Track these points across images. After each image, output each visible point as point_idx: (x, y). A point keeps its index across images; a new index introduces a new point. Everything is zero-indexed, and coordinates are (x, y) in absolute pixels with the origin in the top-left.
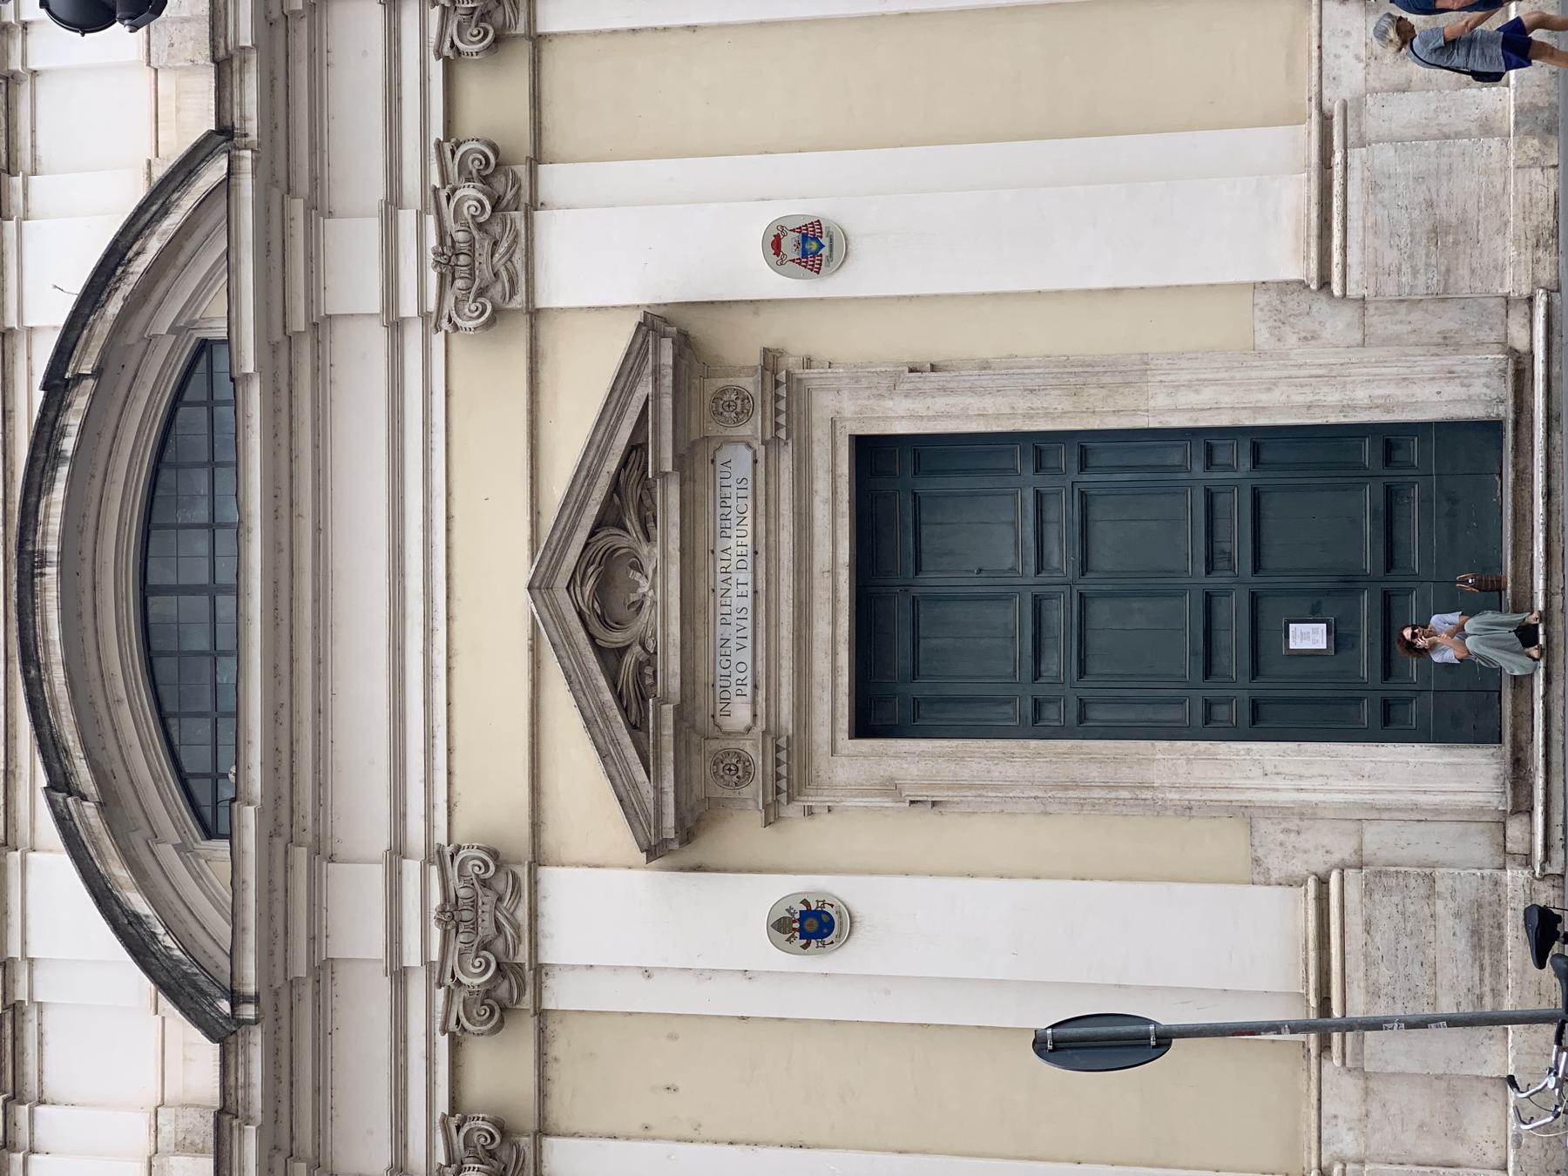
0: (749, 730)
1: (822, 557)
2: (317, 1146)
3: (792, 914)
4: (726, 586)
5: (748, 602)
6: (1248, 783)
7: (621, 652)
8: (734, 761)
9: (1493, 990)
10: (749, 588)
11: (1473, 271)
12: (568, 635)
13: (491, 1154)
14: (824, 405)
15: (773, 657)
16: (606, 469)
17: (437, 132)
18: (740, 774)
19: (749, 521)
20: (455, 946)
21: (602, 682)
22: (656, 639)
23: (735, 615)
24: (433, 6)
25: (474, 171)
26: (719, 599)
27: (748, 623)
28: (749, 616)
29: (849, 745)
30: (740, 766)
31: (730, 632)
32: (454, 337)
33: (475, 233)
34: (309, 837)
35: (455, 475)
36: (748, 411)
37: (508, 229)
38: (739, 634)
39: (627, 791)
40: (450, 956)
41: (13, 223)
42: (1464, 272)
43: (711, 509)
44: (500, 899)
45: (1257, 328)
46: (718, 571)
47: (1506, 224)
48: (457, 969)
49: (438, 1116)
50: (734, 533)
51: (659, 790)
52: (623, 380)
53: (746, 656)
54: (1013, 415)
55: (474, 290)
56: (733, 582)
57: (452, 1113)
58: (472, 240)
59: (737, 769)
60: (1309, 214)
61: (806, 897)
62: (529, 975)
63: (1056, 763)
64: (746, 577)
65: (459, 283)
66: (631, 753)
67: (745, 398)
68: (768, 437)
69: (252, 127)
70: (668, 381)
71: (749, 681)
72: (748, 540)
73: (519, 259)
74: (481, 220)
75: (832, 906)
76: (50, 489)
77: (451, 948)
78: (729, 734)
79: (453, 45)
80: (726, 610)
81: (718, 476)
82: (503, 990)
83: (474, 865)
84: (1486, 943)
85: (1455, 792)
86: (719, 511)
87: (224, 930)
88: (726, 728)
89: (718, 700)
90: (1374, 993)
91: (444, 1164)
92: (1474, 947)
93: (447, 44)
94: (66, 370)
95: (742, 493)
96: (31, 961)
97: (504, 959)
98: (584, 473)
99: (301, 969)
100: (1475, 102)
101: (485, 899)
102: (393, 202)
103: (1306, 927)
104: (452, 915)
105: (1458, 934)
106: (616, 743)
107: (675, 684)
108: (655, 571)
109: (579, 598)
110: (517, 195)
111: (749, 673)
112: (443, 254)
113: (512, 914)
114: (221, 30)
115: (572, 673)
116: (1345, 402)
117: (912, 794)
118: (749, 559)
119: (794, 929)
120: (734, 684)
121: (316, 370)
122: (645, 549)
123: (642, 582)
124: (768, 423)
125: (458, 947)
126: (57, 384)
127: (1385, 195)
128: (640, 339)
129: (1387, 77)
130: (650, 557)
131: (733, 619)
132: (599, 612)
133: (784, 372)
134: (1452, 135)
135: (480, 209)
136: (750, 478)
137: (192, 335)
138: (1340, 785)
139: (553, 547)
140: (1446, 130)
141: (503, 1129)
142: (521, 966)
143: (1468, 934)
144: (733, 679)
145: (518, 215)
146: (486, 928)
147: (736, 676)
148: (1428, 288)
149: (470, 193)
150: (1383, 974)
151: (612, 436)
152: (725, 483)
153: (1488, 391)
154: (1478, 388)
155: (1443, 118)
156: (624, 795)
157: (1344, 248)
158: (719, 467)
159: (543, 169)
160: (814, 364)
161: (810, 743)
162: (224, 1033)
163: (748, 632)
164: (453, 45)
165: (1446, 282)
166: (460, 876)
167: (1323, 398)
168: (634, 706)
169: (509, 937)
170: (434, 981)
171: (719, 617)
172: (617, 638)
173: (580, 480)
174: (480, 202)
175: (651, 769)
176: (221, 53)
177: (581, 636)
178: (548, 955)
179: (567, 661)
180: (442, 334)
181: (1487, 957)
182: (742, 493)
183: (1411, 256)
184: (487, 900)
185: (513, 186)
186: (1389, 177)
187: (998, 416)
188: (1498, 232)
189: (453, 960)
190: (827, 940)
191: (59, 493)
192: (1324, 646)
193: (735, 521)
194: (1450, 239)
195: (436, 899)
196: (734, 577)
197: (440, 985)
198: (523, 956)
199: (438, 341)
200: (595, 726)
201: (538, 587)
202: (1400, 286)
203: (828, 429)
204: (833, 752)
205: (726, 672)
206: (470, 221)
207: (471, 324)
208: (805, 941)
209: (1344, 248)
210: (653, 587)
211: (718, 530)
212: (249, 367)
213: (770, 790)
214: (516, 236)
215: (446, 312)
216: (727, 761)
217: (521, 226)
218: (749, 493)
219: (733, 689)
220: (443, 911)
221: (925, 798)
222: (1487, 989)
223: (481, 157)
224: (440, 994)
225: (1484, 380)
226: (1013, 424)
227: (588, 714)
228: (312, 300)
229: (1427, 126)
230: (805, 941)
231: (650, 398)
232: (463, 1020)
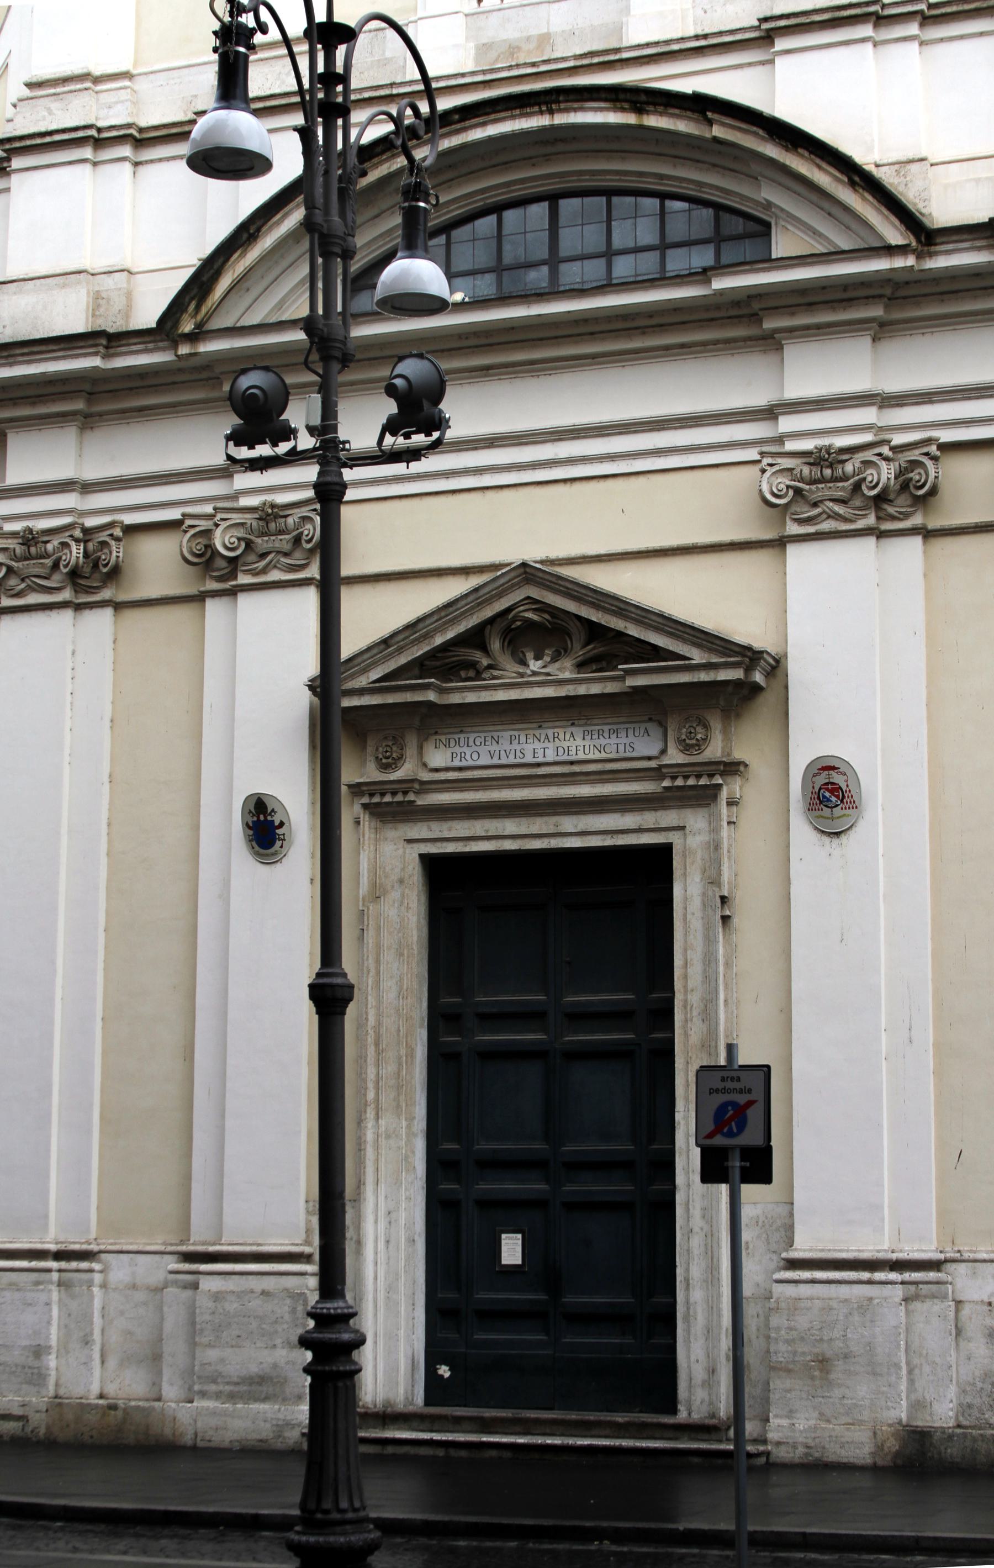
0: (425, 765)
1: (569, 823)
2: (100, 415)
3: (270, 814)
4: (543, 737)
5: (529, 759)
6: (381, 1199)
7: (485, 649)
8: (394, 755)
9: (221, 1392)
10: (540, 759)
11: (789, 1391)
12: (488, 601)
13: (96, 566)
14: (695, 820)
15: (483, 784)
16: (629, 625)
17: (947, 436)
18: (384, 761)
19: (598, 756)
20: (248, 518)
21: (450, 634)
22: (491, 679)
23: (518, 748)
25: (911, 475)
26: (531, 732)
27: (512, 760)
28: (518, 761)
29: (414, 855)
30: (390, 760)
31: (505, 744)
32: (756, 469)
33: (851, 481)
35: (641, 480)
36: (687, 750)
37: (857, 512)
40: (240, 515)
42: (788, 1383)
43: (610, 720)
44: (286, 555)
45: (758, 1206)
46: (556, 730)
47: (828, 1421)
48: (228, 523)
49: (887, 437)
50: (587, 743)
51: (361, 692)
52: (702, 636)
53: (484, 760)
54: (686, 991)
55: (800, 485)
56: (546, 744)
58: (845, 478)
59: (387, 758)
60: (848, 1251)
61: (287, 824)
62: (227, 585)
63: (398, 1035)
65: (806, 470)
66: (392, 665)
67: (698, 746)
68: (664, 770)
70: (704, 676)
71: (464, 763)
72: (581, 756)
73: (827, 526)
74: (864, 487)
75: (281, 847)
76: (615, 109)
77: (10, 541)
78: (422, 748)
80: (523, 739)
81: (636, 725)
84: (254, 1388)
85: (375, 1367)
86: (606, 728)
87: (254, 318)
88: (425, 744)
89: (449, 736)
90: (217, 1297)
91: (893, 443)
92: (251, 1378)
95: (621, 748)
96: (771, 62)
97: (240, 562)
98: (622, 606)
99: (769, 324)
100: (940, 1397)
101: (284, 542)
103: (270, 1245)
105: (261, 1366)
106: (400, 650)
107: (456, 699)
108: (548, 674)
110: (893, 518)
111: (471, 763)
112: (829, 454)
113: (275, 567)
115: (454, 608)
116: (691, 1282)
118: (565, 758)
119: (258, 817)
120: (462, 750)
121: (727, 341)
122: (568, 663)
123: (539, 663)
124: (676, 770)
125: (247, 521)
127: (856, 1318)
128: (737, 649)
129: (973, 1320)
131: (515, 746)
132: (513, 627)
133: (721, 782)
134: (912, 1377)
135: (872, 485)
136: (635, 754)
137: (772, 217)
138: (381, 1274)
139: (560, 582)
140: (917, 1371)
141: (115, 574)
142: (236, 578)
143: (261, 1373)
144: (465, 749)
145: (871, 520)
146: (262, 543)
147: (468, 752)
148: (776, 1353)
149: (886, 473)
150: (232, 1306)
151: (658, 629)
152: (631, 732)
153: (698, 1402)
154: (700, 1395)
155: (927, 1369)
156: (356, 662)
157: (813, 1281)
158: (643, 726)
159: (917, 541)
160: (735, 808)
161: (414, 821)
163: (504, 761)
165: (780, 1369)
167: (695, 1262)
168: (438, 663)
171: (516, 733)
172: (495, 645)
174: (877, 484)
175: (377, 685)
177: (488, 612)
178: (244, 600)
181: (245, 1388)
182: (621, 748)
183: (802, 1339)
184: (283, 542)
185: (900, 513)
186: (872, 1321)
187: (685, 977)
188: (821, 1414)
192: (504, 1262)
193: (597, 742)
194: (817, 1373)
196: (551, 745)
197: (762, 454)
200: (411, 632)
202: (778, 1329)
204: (409, 841)
205: (471, 743)
206: (861, 476)
207: (765, 488)
208: (251, 825)
209: (813, 1281)
210: (534, 674)
211: (589, 728)
213: (372, 788)
214: (851, 521)
215: (779, 460)
216: (395, 748)
217: (860, 524)
218: (622, 755)
219: (457, 750)
220: (273, 506)
221: (366, 923)
222: (221, 1388)
223: (923, 481)
224: (208, 509)
225: (707, 1399)
226: (679, 991)
228: (791, 331)
229: (921, 1355)
230: (251, 825)
232: (192, 532)
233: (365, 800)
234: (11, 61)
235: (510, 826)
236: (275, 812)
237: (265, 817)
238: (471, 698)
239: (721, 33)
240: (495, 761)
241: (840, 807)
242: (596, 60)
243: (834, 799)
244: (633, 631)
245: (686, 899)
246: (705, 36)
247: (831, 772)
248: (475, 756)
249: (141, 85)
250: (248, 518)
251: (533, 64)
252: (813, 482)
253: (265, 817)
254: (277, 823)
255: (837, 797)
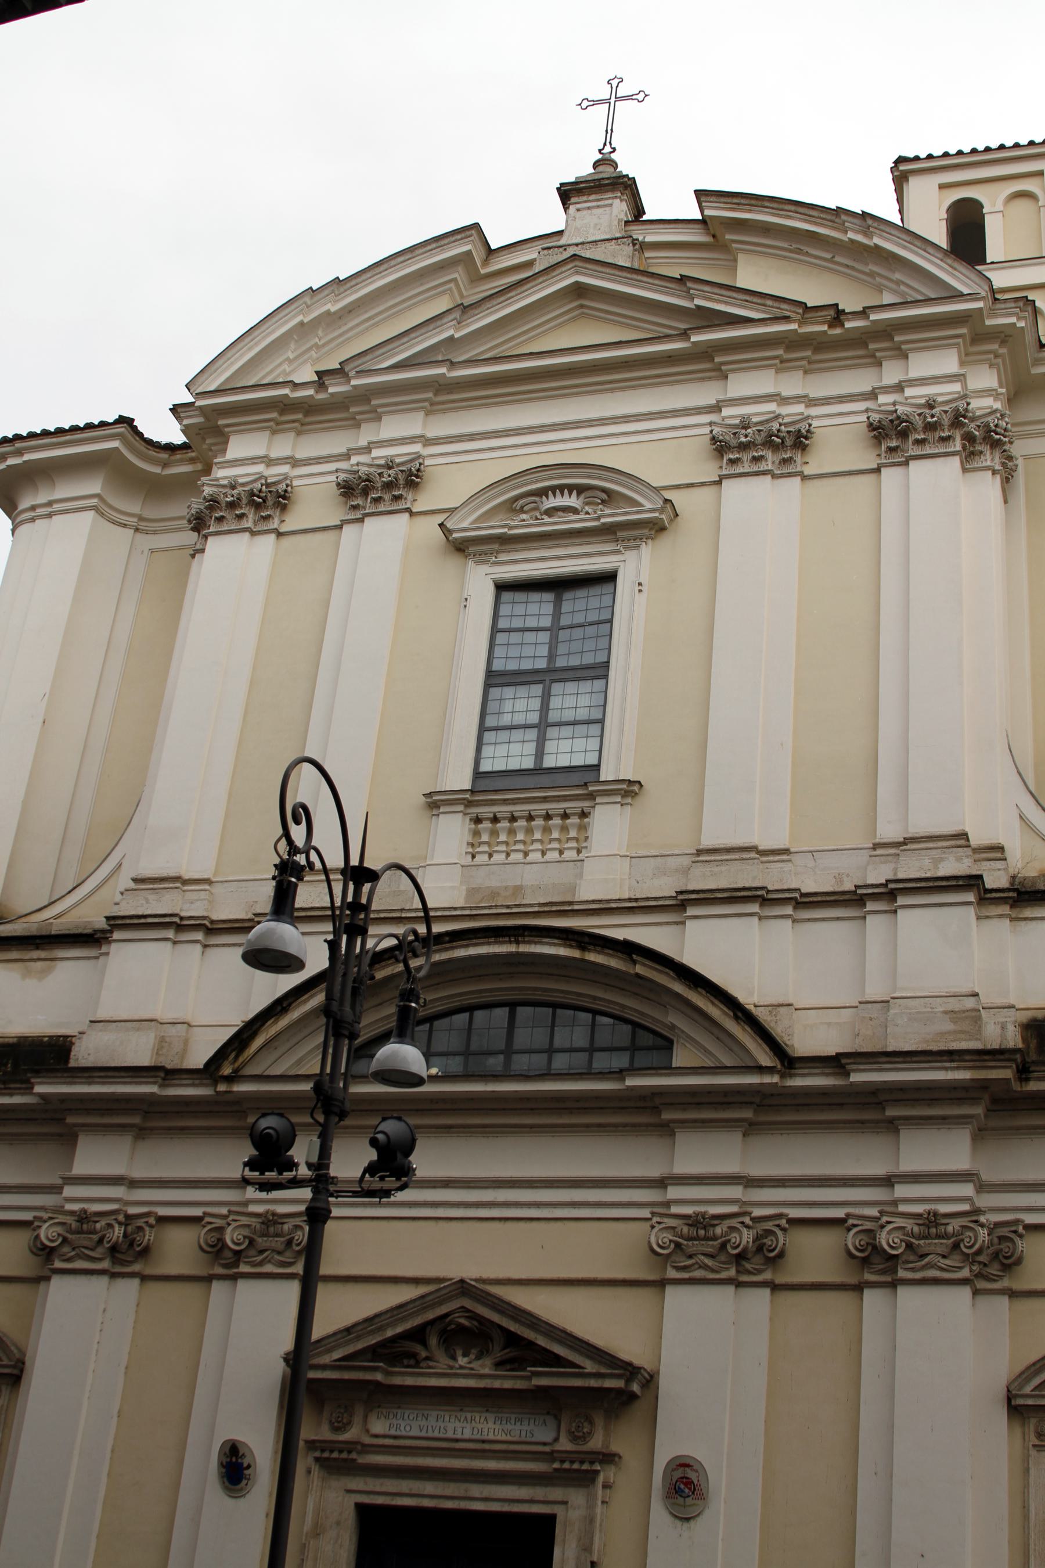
0: (367, 1431)
1: (476, 1490)
2: (152, 1129)
5: (450, 1434)
7: (425, 1345)
10: (459, 1436)
12: (432, 1306)
13: (131, 1244)
14: (576, 1497)
16: (539, 1337)
17: (162, 1211)
18: (336, 1424)
19: (504, 1438)
21: (399, 1329)
24: (879, 1212)
27: (436, 1434)
28: (441, 1435)
30: (341, 1424)
31: (432, 1421)
32: (647, 1225)
34: (762, 1118)
35: (522, 1225)
37: (722, 1265)
38: (430, 1428)
39: (326, 1345)
41: (791, 913)
46: (473, 1414)
48: (238, 1223)
49: (749, 1209)
50: (497, 1427)
53: (415, 1432)
56: (465, 1424)
57: (753, 1219)
58: (714, 1238)
59: (339, 1422)
64: (467, 1434)
65: (685, 1229)
67: (584, 1438)
69: (798, 1082)
70: (593, 1383)
71: (398, 1433)
72: (491, 1437)
73: (698, 1274)
75: (247, 1484)
76: (565, 946)
79: (855, 1226)
82: (876, 1259)
83: (735, 1237)
91: (753, 1215)
93: (856, 1222)
94: (638, 955)
95: (523, 1434)
97: (243, 1254)
101: (279, 1243)
102: (134, 1184)
104: (932, 1221)
106: (358, 1338)
107: (397, 1381)
108: (472, 1369)
109: (457, 1315)
111: (404, 1433)
114: (859, 1060)
117: (311, 1545)
118: (478, 1437)
123: (466, 1359)
126: (629, 949)
130: (483, 1366)
131: (440, 1423)
132: (449, 1328)
136: (533, 1440)
141: (145, 1252)
142: (238, 1267)
149: (746, 1238)
156: (323, 1343)
162: (211, 1070)
163: (430, 1434)
164: (855, 1226)
166: (963, 1227)
169: (255, 1259)
170: (656, 1210)
171: (442, 1413)
172: (433, 1341)
173: (531, 1318)
174: (739, 1245)
176: (843, 1061)
177: (430, 1315)
179: (412, 1306)
180: (649, 1216)
182: (523, 1434)
184: (279, 1243)
185: (755, 1269)
189: (900, 1222)
190: (225, 1480)
191: (562, 951)
195: (944, 1209)
196: (468, 1426)
197: (880, 1212)
198: (244, 1268)
199: (645, 1213)
201: (463, 1287)
203: (560, 1498)
206: (727, 1238)
207: (653, 1240)
210: (461, 1367)
212: (856, 1077)
215: (666, 1220)
217: (724, 1275)
218: (523, 1439)
219: (394, 1421)
220: (274, 1214)
227: (377, 1320)
228: (909, 1120)
231: (581, 1370)
233: (318, 1454)
234: (124, 862)
235: (429, 1487)
236: (245, 1457)
237: (237, 1460)
238: (410, 1381)
239: (648, 899)
240: (423, 1434)
241: (691, 1498)
242: (554, 908)
243: (687, 1490)
244: (542, 1341)
245: (563, 1561)
246: (636, 900)
247: (687, 1469)
248: (408, 1428)
249: (217, 889)
250: (908, 1224)
251: (508, 907)
252: (690, 1239)
253: (237, 1460)
254: (245, 1465)
255: (690, 1489)
